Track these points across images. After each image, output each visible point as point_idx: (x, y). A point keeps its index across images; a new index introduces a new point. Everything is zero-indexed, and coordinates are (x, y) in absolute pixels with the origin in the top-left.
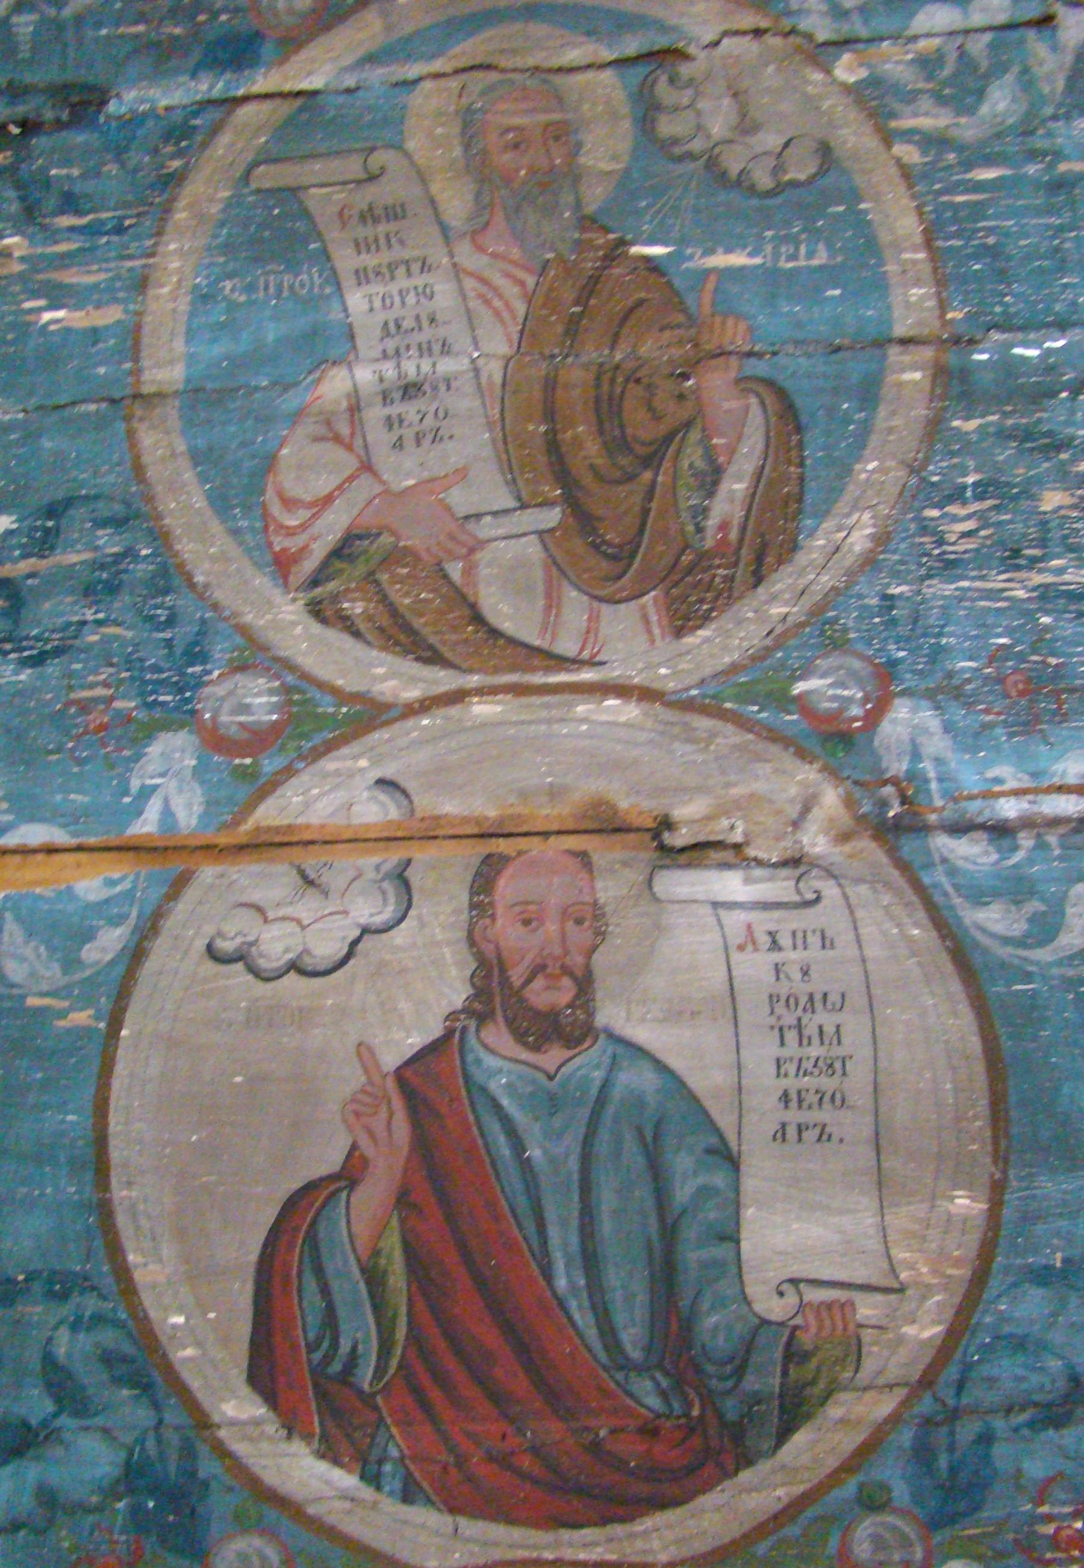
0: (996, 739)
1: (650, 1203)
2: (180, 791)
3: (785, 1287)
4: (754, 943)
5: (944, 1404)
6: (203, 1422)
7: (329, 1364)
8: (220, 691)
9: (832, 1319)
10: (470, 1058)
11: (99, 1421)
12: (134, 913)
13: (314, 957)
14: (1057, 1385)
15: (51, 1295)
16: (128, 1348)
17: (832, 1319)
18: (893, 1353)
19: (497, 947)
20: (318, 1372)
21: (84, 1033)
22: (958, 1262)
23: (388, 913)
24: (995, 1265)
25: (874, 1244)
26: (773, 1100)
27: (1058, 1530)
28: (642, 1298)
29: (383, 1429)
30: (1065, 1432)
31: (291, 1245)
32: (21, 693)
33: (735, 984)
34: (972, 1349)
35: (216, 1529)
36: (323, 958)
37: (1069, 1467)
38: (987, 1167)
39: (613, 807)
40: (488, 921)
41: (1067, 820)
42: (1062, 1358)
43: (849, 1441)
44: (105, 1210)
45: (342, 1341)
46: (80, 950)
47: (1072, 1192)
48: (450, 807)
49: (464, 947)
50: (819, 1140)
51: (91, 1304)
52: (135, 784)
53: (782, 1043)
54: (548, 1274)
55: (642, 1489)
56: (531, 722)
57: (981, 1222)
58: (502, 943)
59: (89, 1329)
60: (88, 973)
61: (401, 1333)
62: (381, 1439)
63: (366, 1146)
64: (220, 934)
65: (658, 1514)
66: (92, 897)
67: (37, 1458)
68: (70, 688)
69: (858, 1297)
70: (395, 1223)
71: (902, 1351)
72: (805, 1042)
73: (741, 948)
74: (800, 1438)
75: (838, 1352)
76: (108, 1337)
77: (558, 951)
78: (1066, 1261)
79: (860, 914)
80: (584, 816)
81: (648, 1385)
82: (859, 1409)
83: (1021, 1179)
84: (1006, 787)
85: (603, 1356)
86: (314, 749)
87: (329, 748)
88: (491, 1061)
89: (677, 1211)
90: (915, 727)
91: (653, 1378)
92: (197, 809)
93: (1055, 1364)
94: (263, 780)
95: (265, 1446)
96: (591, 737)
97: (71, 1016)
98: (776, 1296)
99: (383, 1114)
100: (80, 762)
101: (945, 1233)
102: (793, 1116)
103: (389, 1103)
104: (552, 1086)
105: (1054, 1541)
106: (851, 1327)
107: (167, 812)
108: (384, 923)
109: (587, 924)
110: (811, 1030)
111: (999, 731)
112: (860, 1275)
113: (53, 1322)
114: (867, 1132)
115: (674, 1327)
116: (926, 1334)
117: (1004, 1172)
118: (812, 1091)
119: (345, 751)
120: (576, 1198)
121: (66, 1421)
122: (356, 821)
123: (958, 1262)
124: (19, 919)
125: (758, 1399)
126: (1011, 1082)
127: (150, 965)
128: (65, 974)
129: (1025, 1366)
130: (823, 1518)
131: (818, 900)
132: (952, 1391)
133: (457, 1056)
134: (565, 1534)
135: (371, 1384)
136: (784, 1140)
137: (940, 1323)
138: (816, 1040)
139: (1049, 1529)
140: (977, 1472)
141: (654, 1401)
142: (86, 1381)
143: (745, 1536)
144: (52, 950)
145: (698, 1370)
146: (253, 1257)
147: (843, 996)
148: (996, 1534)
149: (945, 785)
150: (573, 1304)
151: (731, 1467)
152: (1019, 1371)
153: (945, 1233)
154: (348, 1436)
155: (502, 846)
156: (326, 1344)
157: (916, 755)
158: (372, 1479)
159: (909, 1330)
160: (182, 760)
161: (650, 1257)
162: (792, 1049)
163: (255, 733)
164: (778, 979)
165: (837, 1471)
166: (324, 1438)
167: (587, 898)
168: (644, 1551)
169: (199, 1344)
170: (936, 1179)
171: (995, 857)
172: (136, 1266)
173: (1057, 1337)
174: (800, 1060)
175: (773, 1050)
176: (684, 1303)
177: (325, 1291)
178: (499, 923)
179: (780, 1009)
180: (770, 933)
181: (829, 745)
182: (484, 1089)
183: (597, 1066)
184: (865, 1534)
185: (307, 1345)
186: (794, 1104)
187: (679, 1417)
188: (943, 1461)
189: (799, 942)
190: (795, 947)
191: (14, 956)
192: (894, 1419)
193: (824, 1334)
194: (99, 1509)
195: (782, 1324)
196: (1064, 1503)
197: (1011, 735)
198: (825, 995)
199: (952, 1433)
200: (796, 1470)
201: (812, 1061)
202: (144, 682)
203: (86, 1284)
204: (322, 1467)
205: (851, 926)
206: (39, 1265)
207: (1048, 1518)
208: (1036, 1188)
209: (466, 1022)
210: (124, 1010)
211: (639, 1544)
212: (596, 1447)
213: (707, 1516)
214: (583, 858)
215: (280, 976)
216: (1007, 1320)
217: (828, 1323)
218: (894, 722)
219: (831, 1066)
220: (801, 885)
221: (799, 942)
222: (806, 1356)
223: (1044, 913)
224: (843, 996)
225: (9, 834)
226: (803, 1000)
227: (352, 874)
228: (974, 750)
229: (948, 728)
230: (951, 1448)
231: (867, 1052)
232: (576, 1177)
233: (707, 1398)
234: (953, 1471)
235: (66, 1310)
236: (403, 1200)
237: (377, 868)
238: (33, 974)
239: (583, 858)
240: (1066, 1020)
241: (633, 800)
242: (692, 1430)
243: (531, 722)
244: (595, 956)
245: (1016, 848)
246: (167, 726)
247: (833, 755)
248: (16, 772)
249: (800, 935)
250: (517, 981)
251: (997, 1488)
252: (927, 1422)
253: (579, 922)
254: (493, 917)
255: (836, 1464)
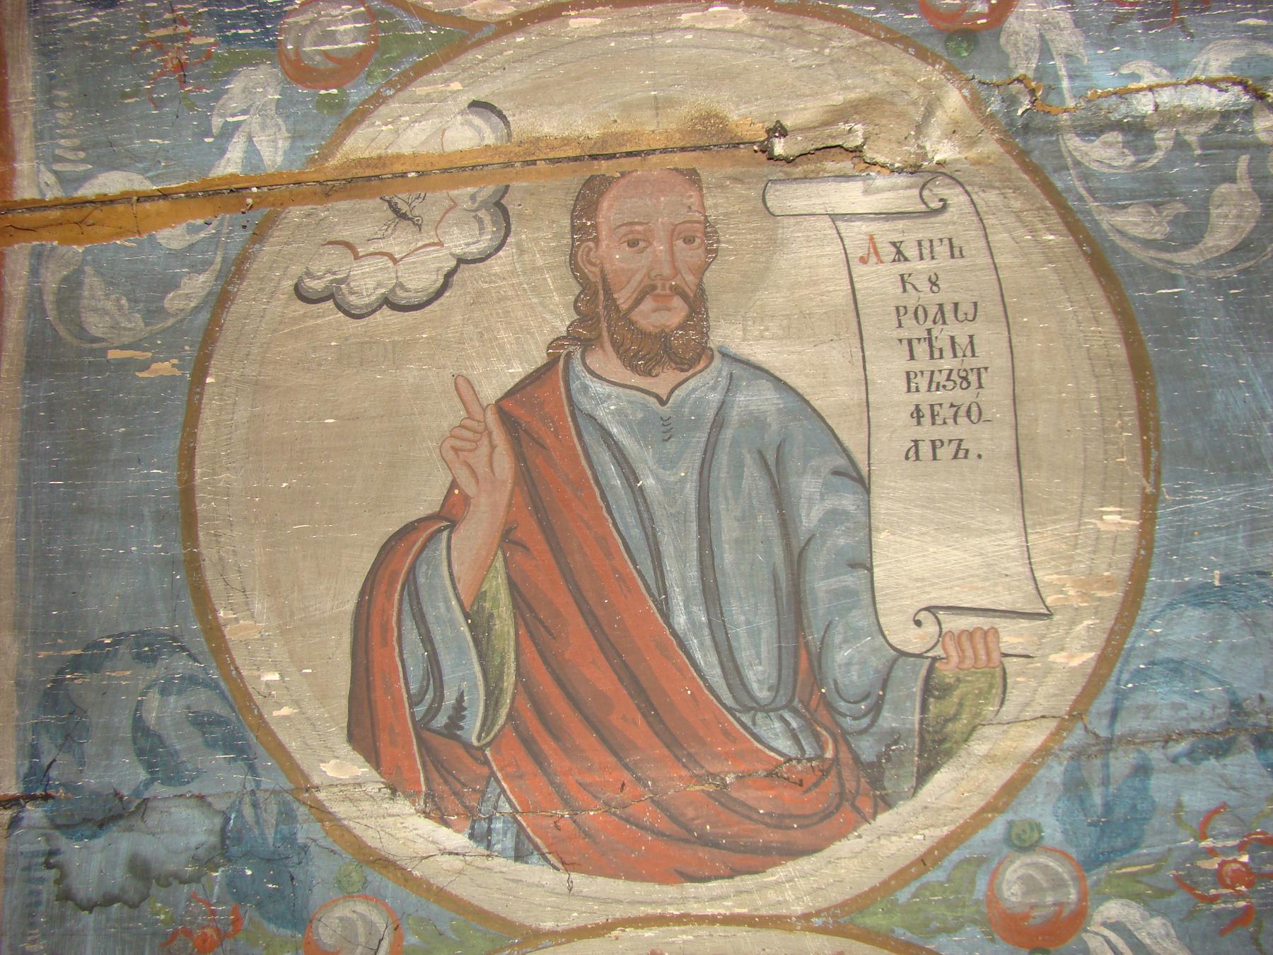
0: (1131, 32)
1: (774, 532)
2: (264, 127)
3: (923, 616)
4: (877, 253)
5: (1097, 736)
6: (302, 785)
7: (434, 716)
8: (302, 19)
9: (974, 648)
10: (575, 385)
11: (195, 788)
12: (219, 259)
13: (407, 290)
14: (1218, 711)
15: (139, 657)
16: (220, 709)
17: (974, 648)
18: (1040, 684)
19: (602, 271)
20: (422, 726)
21: (168, 383)
22: (1109, 583)
23: (485, 242)
24: (1148, 585)
25: (1020, 568)
26: (904, 415)
27: (1222, 864)
28: (768, 635)
29: (493, 783)
30: (1228, 760)
31: (389, 598)
32: (93, 37)
33: (859, 297)
34: (1125, 676)
35: (318, 895)
36: (417, 291)
37: (1232, 797)
38: (1136, 481)
39: (723, 119)
40: (591, 244)
41: (1211, 114)
42: (1221, 683)
43: (995, 778)
44: (193, 564)
45: (446, 693)
46: (162, 299)
47: (1230, 504)
48: (550, 127)
49: (566, 271)
50: (955, 457)
51: (182, 665)
52: (217, 122)
53: (912, 357)
54: (666, 616)
55: (774, 836)
56: (632, 34)
57: (1130, 542)
58: (607, 266)
59: (180, 692)
60: (171, 321)
61: (509, 681)
62: (493, 790)
63: (468, 485)
64: (309, 274)
65: (790, 863)
66: (175, 245)
67: (130, 829)
68: (146, 28)
69: (1001, 624)
70: (499, 563)
71: (1050, 680)
72: (937, 355)
73: (863, 260)
74: (942, 777)
75: (983, 685)
76: (201, 699)
77: (667, 271)
78: (1225, 578)
79: (990, 221)
80: (694, 131)
81: (777, 725)
82: (1006, 745)
83: (1173, 492)
84: (1143, 84)
85: (729, 701)
86: (404, 74)
87: (420, 71)
88: (597, 387)
89: (803, 538)
90: (1045, 22)
91: (783, 719)
92: (282, 144)
93: (1214, 690)
94: (350, 110)
95: (366, 806)
96: (697, 47)
97: (154, 366)
98: (913, 626)
99: (484, 449)
100: (158, 104)
101: (1094, 552)
102: (927, 431)
103: (490, 434)
104: (665, 411)
105: (1219, 877)
106: (995, 655)
107: (252, 152)
108: (480, 253)
109: (698, 241)
110: (942, 342)
111: (1135, 23)
112: (1004, 600)
113: (142, 686)
114: (1008, 445)
115: (804, 664)
116: (1075, 662)
117: (1157, 486)
118: (946, 406)
119: (437, 74)
120: (694, 527)
121: (160, 789)
122: (449, 148)
123: (1109, 583)
124: (99, 272)
125: (895, 737)
126: (1160, 389)
127: (237, 308)
128: (147, 324)
129: (1182, 693)
130: (967, 861)
131: (944, 208)
132: (1105, 722)
133: (561, 384)
134: (691, 888)
135: (479, 738)
136: (917, 458)
137: (1091, 649)
138: (948, 353)
139: (1213, 864)
140: (1134, 807)
141: (785, 745)
142: (178, 747)
143: (885, 883)
144: (134, 301)
145: (831, 708)
146: (350, 606)
147: (975, 304)
148: (1151, 872)
149: (1077, 83)
150: (694, 643)
151: (868, 810)
152: (1177, 699)
153: (1094, 552)
154: (455, 794)
155: (603, 167)
156: (429, 696)
157: (1045, 51)
158: (483, 837)
159: (1058, 658)
160: (264, 94)
161: (777, 589)
162: (923, 362)
163: (338, 61)
164: (905, 290)
165: (983, 810)
166: (430, 796)
167: (698, 217)
168: (779, 903)
169: (296, 703)
170: (1082, 496)
171: (1131, 159)
172: (228, 621)
173: (1215, 661)
174: (932, 372)
175: (900, 363)
176: (814, 637)
177: (427, 640)
178: (604, 244)
179: (908, 321)
180: (894, 244)
181: (952, 45)
182: (591, 418)
183: (713, 389)
184: (1015, 876)
185: (410, 697)
186: (927, 420)
187: (810, 760)
188: (1097, 798)
189: (926, 252)
190: (922, 258)
191: (95, 310)
192: (1044, 752)
193: (968, 663)
194: (194, 880)
195: (920, 656)
196: (1227, 836)
197: (1148, 27)
198: (956, 305)
199: (1106, 766)
200: (938, 811)
201: (945, 373)
202: (222, 16)
203: (176, 644)
204: (427, 826)
205: (981, 233)
206: (125, 628)
207: (1211, 852)
208: (1190, 502)
209: (571, 348)
210: (209, 357)
211: (772, 895)
212: (721, 796)
213: (843, 863)
214: (692, 177)
215: (374, 311)
216: (1165, 645)
217: (969, 653)
218: (1021, 17)
219: (965, 378)
220: (926, 193)
221: (926, 252)
222: (946, 690)
223: (1187, 215)
224: (975, 304)
225: (87, 185)
226: (933, 311)
227: (447, 203)
228: (1107, 44)
229: (1079, 21)
230: (1105, 782)
231: (1004, 362)
232: (693, 507)
233: (842, 737)
234: (1108, 807)
235: (157, 672)
236: (508, 539)
237: (473, 197)
238: (115, 326)
239: (692, 177)
240: (1216, 324)
241: (743, 109)
242: (825, 773)
243: (632, 34)
244: (707, 274)
245: (1152, 149)
246: (248, 62)
247: (958, 54)
248: (92, 120)
249: (926, 244)
250: (624, 305)
251: (1155, 822)
252: (1079, 754)
253: (689, 240)
254: (597, 240)
255: (982, 804)
